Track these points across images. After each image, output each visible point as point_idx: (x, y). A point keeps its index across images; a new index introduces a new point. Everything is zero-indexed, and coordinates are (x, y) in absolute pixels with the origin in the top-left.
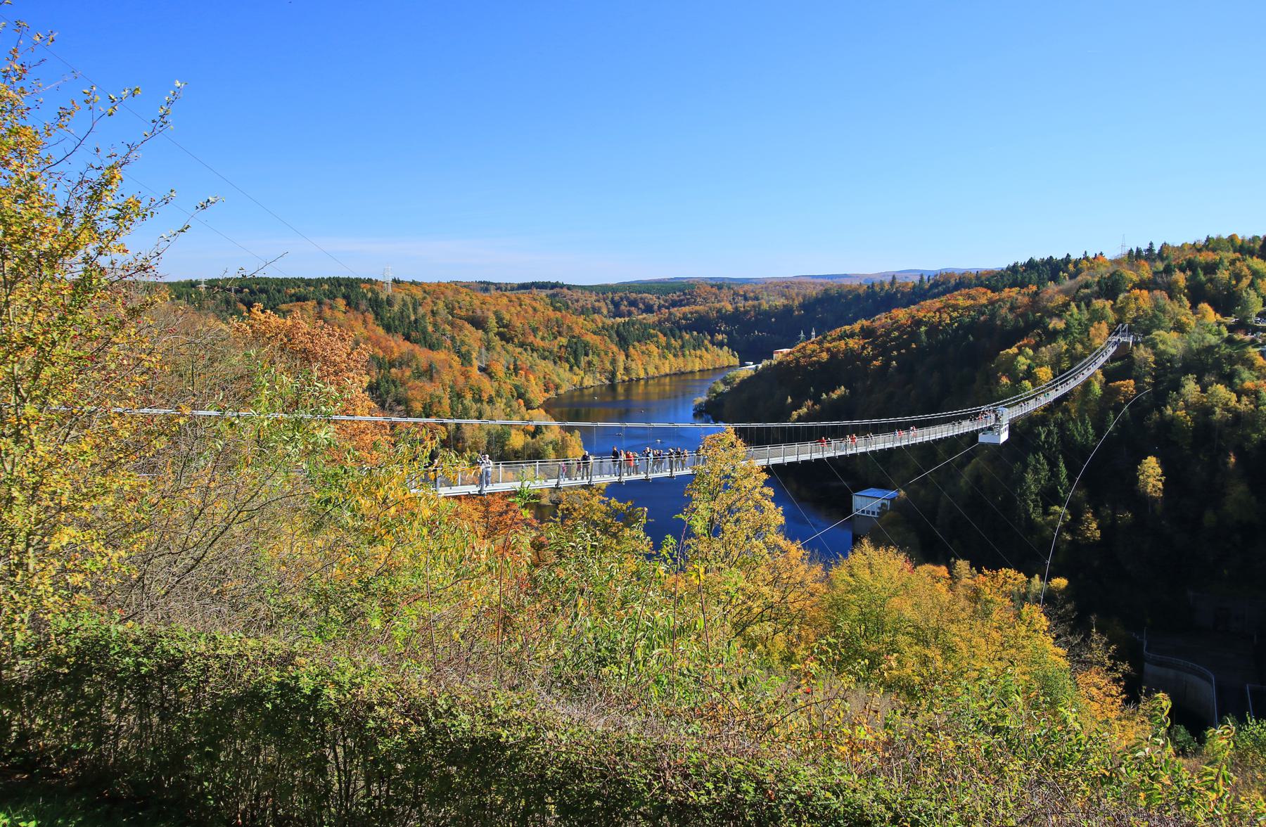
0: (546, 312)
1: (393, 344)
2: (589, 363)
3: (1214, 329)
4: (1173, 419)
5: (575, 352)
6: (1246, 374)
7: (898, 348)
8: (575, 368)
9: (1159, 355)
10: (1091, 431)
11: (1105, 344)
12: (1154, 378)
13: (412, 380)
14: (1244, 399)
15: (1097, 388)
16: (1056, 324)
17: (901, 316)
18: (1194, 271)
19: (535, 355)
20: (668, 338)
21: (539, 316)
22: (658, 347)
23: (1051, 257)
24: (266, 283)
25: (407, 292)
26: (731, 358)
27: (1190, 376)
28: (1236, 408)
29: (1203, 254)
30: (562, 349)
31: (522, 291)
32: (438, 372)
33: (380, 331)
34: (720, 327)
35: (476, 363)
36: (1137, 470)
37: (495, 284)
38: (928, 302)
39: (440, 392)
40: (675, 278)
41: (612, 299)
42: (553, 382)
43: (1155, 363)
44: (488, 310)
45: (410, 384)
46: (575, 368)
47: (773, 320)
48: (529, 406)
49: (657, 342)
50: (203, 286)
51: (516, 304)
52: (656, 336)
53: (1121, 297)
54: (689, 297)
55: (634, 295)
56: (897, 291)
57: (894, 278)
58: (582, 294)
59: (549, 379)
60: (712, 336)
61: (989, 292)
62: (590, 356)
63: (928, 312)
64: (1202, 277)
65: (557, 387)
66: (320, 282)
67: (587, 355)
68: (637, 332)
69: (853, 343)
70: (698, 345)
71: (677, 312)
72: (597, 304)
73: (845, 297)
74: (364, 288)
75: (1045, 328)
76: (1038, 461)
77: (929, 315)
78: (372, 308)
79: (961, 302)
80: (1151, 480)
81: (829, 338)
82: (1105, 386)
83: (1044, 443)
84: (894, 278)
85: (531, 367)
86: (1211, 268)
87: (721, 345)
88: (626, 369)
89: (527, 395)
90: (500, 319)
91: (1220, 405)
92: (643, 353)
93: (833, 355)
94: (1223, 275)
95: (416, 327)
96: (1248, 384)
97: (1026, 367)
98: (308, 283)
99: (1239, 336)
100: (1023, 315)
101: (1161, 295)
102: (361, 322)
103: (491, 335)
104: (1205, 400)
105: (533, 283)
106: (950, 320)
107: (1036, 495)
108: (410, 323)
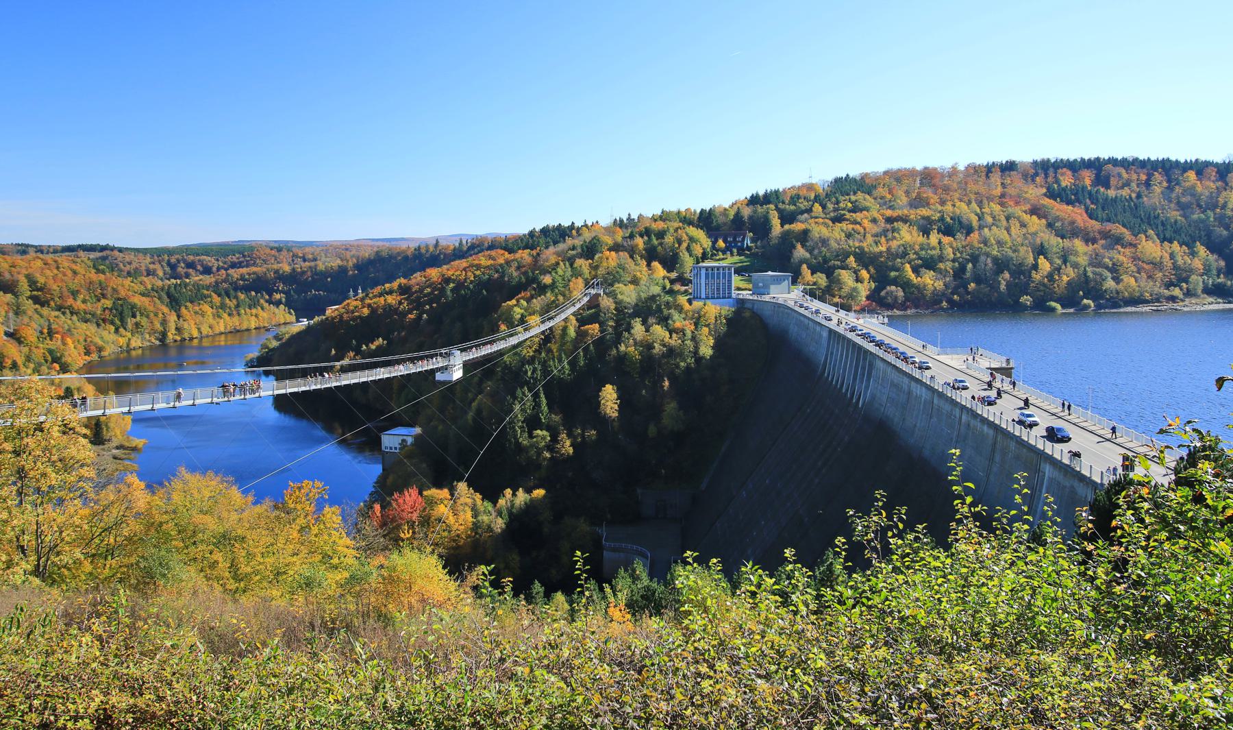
2: (137, 325)
5: (121, 314)
6: (676, 316)
8: (121, 330)
9: (618, 303)
10: (567, 366)
11: (580, 294)
14: (674, 335)
15: (572, 332)
16: (547, 280)
17: (433, 274)
18: (649, 236)
20: (223, 298)
22: (212, 308)
30: (107, 311)
31: (67, 254)
34: (278, 287)
36: (599, 396)
37: (36, 247)
38: (457, 262)
41: (169, 261)
42: (95, 345)
46: (121, 330)
47: (329, 279)
48: (65, 369)
49: (211, 302)
52: (210, 296)
54: (248, 259)
55: (191, 258)
56: (440, 253)
57: (437, 240)
58: (135, 256)
60: (270, 295)
61: (507, 253)
64: (655, 242)
65: (100, 349)
67: (134, 316)
68: (190, 293)
69: (391, 300)
70: (254, 304)
71: (235, 273)
72: (151, 266)
73: (395, 258)
75: (539, 283)
76: (524, 394)
77: (456, 273)
80: (609, 403)
81: (371, 295)
83: (530, 378)
84: (437, 240)
85: (69, 330)
86: (661, 235)
87: (278, 303)
88: (177, 329)
89: (63, 360)
90: (32, 283)
92: (196, 313)
93: (373, 311)
94: (669, 239)
96: (678, 324)
97: (519, 316)
99: (677, 287)
100: (525, 273)
101: (624, 255)
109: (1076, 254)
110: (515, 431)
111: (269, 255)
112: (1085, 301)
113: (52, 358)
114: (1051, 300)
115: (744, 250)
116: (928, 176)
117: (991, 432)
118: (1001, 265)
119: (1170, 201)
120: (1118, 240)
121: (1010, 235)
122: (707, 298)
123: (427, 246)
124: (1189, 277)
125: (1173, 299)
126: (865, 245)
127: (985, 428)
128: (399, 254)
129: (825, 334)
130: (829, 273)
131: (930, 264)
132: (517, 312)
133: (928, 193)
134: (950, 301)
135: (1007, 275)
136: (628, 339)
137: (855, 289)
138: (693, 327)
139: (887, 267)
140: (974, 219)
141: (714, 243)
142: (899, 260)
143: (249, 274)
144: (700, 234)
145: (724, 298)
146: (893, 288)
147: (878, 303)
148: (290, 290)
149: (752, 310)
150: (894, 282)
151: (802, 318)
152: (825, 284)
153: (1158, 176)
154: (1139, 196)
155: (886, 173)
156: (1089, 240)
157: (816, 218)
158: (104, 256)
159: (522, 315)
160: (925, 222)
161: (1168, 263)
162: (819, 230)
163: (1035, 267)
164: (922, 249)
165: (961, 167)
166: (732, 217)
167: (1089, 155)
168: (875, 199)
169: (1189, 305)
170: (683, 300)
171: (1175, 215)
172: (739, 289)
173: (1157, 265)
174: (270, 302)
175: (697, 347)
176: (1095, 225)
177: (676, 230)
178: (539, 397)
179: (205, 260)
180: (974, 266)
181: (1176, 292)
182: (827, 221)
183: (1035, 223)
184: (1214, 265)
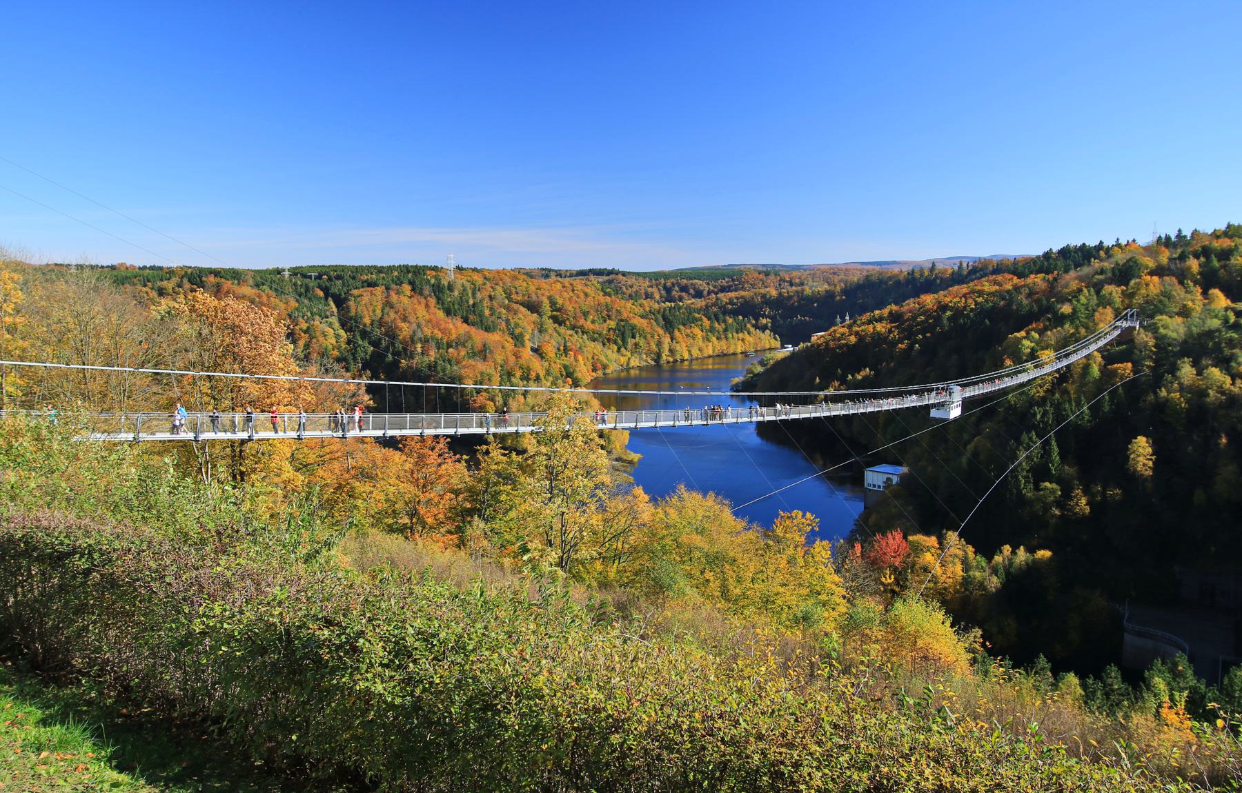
0: (597, 297)
1: (451, 326)
2: (636, 345)
3: (1220, 314)
4: (1167, 400)
5: (623, 335)
7: (923, 332)
8: (623, 349)
11: (1108, 328)
12: (1155, 361)
13: (466, 359)
15: (1095, 371)
16: (1066, 309)
17: (928, 301)
19: (585, 337)
20: (712, 322)
21: (590, 301)
22: (702, 331)
23: (1084, 244)
24: (343, 271)
25: (469, 278)
26: (773, 341)
27: (1186, 359)
28: (1231, 391)
29: (1220, 241)
30: (611, 332)
32: (491, 352)
33: (441, 314)
34: (764, 312)
35: (529, 345)
36: (1128, 449)
37: (556, 271)
39: (492, 371)
40: (729, 265)
41: (665, 284)
42: (601, 362)
43: (1156, 346)
44: (543, 295)
45: (464, 363)
46: (623, 349)
48: (576, 384)
49: (701, 325)
50: (287, 273)
51: (569, 290)
52: (701, 320)
53: (1133, 282)
54: (737, 283)
55: (685, 281)
56: (936, 277)
59: (598, 359)
60: (757, 320)
61: (1015, 278)
62: (637, 339)
63: (955, 297)
65: (605, 367)
66: (390, 269)
67: (634, 337)
68: (682, 316)
69: (880, 327)
70: (741, 329)
72: (650, 289)
73: (886, 283)
74: (430, 275)
75: (1055, 313)
76: (1031, 439)
77: (955, 300)
78: (435, 293)
79: (987, 287)
81: (859, 322)
82: (1103, 370)
83: (1039, 422)
85: (580, 348)
86: (1225, 255)
87: (764, 328)
88: (670, 350)
89: (575, 375)
90: (553, 303)
91: (1215, 388)
92: (688, 336)
95: (474, 311)
97: (1029, 350)
98: (380, 270)
101: (1171, 280)
102: (423, 305)
103: (545, 318)
104: (1201, 383)
105: (590, 270)
106: (975, 305)
107: (1028, 472)
108: (469, 307)
110: (1018, 481)
123: (922, 270)
128: (890, 278)
143: (738, 298)
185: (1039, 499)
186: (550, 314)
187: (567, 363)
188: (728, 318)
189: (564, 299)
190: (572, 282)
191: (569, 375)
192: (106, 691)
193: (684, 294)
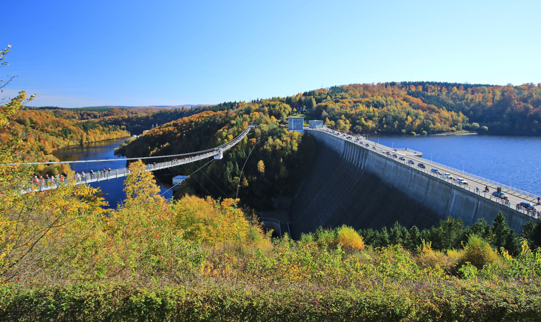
2: (72, 137)
4: (266, 149)
5: (65, 133)
6: (284, 136)
7: (185, 130)
8: (66, 139)
9: (262, 131)
10: (245, 154)
11: (248, 129)
12: (261, 137)
15: (246, 141)
16: (233, 122)
18: (270, 107)
19: (48, 134)
20: (103, 127)
22: (99, 131)
26: (128, 134)
30: (60, 132)
36: (257, 165)
37: (29, 107)
38: (195, 115)
42: (56, 144)
44: (26, 117)
46: (66, 139)
49: (99, 129)
52: (99, 127)
55: (89, 112)
56: (184, 111)
60: (120, 126)
64: (272, 109)
65: (58, 146)
67: (70, 134)
69: (171, 128)
70: (115, 130)
71: (107, 118)
72: (74, 115)
75: (230, 123)
76: (230, 163)
79: (205, 115)
81: (162, 127)
82: (248, 140)
85: (46, 139)
86: (274, 106)
87: (123, 129)
88: (87, 139)
90: (31, 121)
92: (94, 133)
93: (164, 132)
94: (277, 108)
96: (285, 139)
99: (282, 125)
101: (261, 113)
103: (28, 127)
109: (420, 115)
110: (227, 177)
111: (118, 111)
112: (424, 131)
113: (41, 149)
114: (412, 131)
115: (303, 112)
116: (366, 87)
117: (427, 179)
118: (395, 118)
119: (449, 97)
120: (433, 111)
121: (397, 108)
122: (294, 129)
123: (179, 109)
124: (458, 123)
125: (453, 131)
126: (347, 111)
127: (424, 177)
128: (169, 112)
129: (343, 143)
130: (336, 120)
131: (370, 118)
132: (224, 134)
133: (367, 93)
134: (378, 131)
135: (397, 122)
136: (267, 144)
137: (345, 127)
138: (290, 140)
139: (355, 119)
140: (384, 102)
141: (293, 109)
142: (359, 116)
143: (112, 118)
144: (288, 106)
145: (300, 129)
146: (358, 126)
147: (353, 131)
148: (127, 125)
149: (310, 134)
150: (358, 124)
151: (331, 137)
152: (334, 125)
153: (444, 88)
154: (438, 95)
155: (350, 85)
156: (424, 110)
157: (329, 101)
158: (56, 110)
159: (226, 135)
160: (367, 103)
161: (451, 119)
162: (331, 105)
163: (407, 119)
164: (367, 113)
165: (375, 84)
166: (298, 100)
167: (420, 80)
168: (349, 94)
169: (458, 133)
170: (285, 130)
171: (451, 102)
172: (304, 126)
173: (447, 119)
174: (121, 129)
175: (292, 147)
176: (425, 105)
177: (279, 105)
178: (236, 165)
179: (94, 113)
180: (386, 119)
181: (454, 129)
182: (333, 102)
183: (405, 104)
184: (465, 119)
185: (234, 183)
186: (30, 125)
187: (40, 145)
188: (110, 126)
189: (37, 119)
190: (40, 112)
191: (42, 150)
192: (262, 313)
193: (89, 117)
